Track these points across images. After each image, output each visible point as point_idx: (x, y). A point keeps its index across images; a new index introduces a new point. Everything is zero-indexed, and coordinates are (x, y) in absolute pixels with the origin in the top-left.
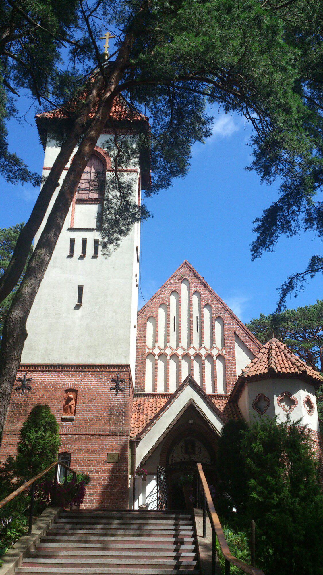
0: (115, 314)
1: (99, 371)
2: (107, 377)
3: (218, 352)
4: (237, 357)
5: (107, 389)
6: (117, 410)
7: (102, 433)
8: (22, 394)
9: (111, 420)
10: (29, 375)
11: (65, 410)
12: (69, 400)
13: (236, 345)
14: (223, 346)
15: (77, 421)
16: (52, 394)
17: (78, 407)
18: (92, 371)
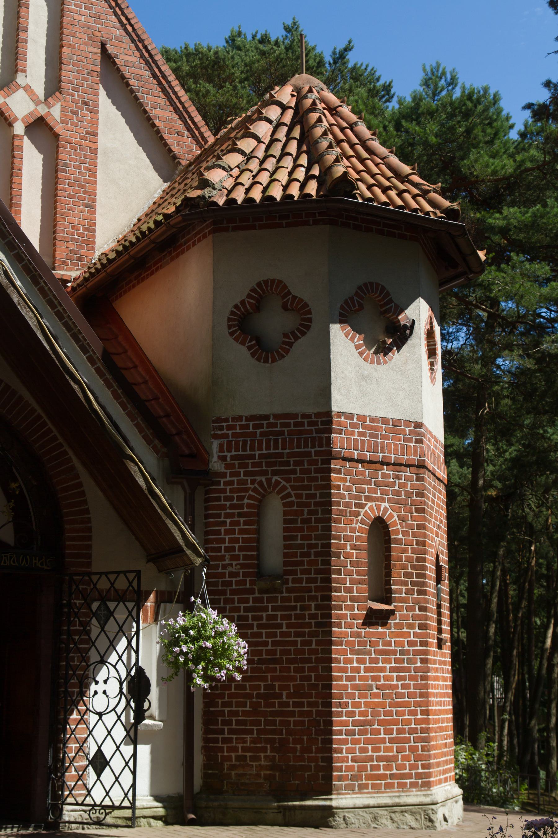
3: (32, 107)
4: (104, 141)
13: (105, 103)
14: (54, 85)
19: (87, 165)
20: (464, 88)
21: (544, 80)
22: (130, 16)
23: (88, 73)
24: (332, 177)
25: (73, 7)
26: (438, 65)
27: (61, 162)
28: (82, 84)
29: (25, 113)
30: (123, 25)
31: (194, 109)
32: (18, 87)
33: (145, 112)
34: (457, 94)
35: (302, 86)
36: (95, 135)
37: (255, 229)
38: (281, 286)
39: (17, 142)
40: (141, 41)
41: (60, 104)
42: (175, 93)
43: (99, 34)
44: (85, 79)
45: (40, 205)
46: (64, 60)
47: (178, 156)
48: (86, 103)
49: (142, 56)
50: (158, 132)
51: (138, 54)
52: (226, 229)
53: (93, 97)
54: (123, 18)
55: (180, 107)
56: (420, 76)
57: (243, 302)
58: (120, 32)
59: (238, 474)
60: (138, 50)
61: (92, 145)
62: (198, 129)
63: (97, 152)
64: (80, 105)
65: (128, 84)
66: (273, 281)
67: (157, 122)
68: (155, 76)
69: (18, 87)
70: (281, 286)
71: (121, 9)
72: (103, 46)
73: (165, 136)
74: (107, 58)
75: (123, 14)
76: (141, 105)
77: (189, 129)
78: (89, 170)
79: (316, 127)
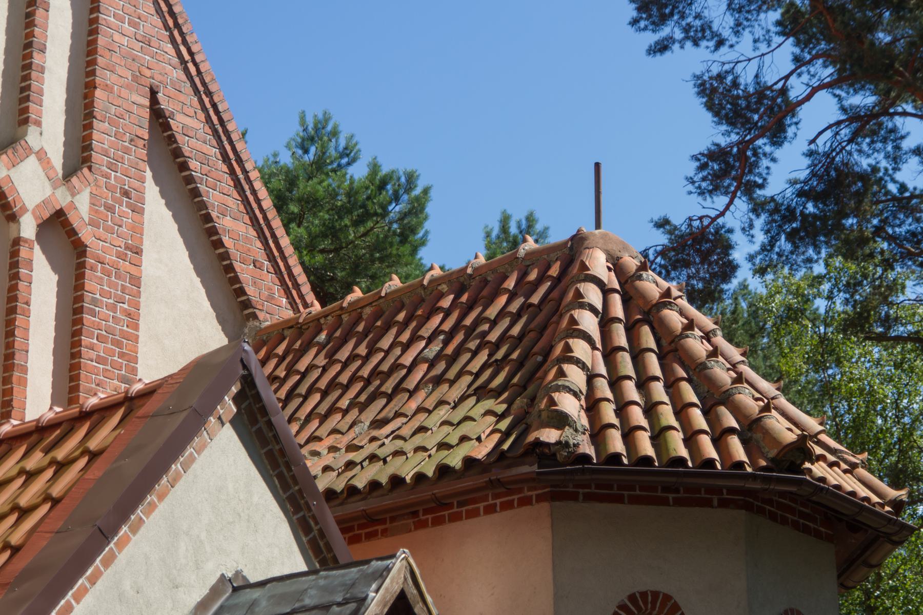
13: (152, 194)
14: (79, 156)
19: (125, 306)
22: (194, 49)
23: (131, 140)
24: (721, 425)
25: (112, 19)
26: (327, 120)
27: (88, 296)
28: (123, 158)
29: (38, 200)
30: (183, 62)
31: (280, 224)
32: (29, 151)
33: (208, 218)
35: (619, 254)
36: (138, 252)
37: (623, 502)
38: (669, 604)
39: (24, 252)
40: (209, 94)
41: (88, 190)
42: (254, 192)
43: (148, 73)
44: (127, 151)
45: (50, 367)
46: (97, 111)
47: (254, 303)
48: (126, 194)
49: (208, 119)
50: (226, 256)
51: (202, 116)
52: (573, 497)
53: (136, 184)
54: (183, 49)
55: (260, 216)
56: (294, 130)
60: (202, 110)
61: (133, 270)
62: (284, 259)
63: (140, 283)
64: (118, 195)
65: (184, 167)
66: (655, 594)
67: (226, 240)
68: (225, 158)
69: (29, 151)
70: (669, 604)
71: (182, 34)
72: (153, 93)
73: (237, 266)
74: (159, 119)
75: (185, 42)
76: (203, 205)
77: (271, 258)
78: (129, 315)
79: (687, 337)
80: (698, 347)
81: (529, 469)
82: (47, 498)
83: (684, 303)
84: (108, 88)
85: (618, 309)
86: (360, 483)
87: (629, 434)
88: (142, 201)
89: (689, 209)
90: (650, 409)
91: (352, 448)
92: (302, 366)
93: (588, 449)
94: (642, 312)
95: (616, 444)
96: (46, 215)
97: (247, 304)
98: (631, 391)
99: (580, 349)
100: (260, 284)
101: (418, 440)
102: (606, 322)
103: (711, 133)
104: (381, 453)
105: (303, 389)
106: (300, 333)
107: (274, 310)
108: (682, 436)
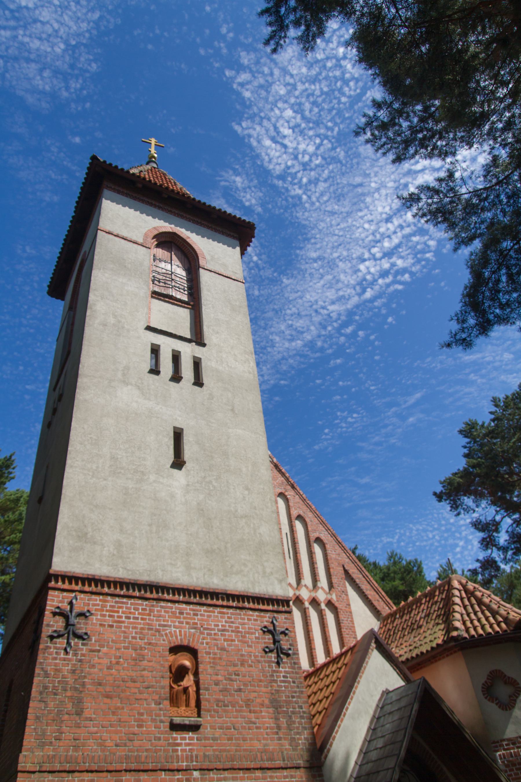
0: (246, 492)
1: (237, 608)
2: (253, 622)
4: (353, 607)
5: (257, 650)
6: (288, 702)
7: (267, 764)
8: (67, 653)
9: (279, 728)
10: (82, 602)
11: (174, 700)
12: (179, 673)
14: (331, 586)
15: (206, 731)
16: (142, 658)
17: (205, 695)
18: (223, 606)
20: (406, 560)
21: (476, 559)
32: (319, 588)
33: (363, 592)
34: (404, 562)
36: (349, 605)
50: (370, 601)
57: (486, 682)
58: (347, 560)
59: (513, 770)
65: (355, 581)
67: (369, 596)
69: (319, 588)
74: (346, 572)
80: (486, 600)
81: (452, 644)
82: (338, 678)
83: (481, 588)
84: (333, 568)
85: (464, 595)
86: (414, 655)
87: (475, 628)
88: (347, 592)
89: (482, 555)
90: (479, 620)
91: (410, 645)
92: (395, 625)
93: (466, 635)
94: (470, 594)
95: (473, 632)
96: (326, 602)
97: (378, 611)
98: (473, 616)
99: (457, 608)
100: (380, 605)
101: (425, 640)
102: (462, 599)
103: (481, 535)
104: (417, 645)
105: (396, 631)
106: (392, 615)
107: (385, 611)
108: (488, 626)
